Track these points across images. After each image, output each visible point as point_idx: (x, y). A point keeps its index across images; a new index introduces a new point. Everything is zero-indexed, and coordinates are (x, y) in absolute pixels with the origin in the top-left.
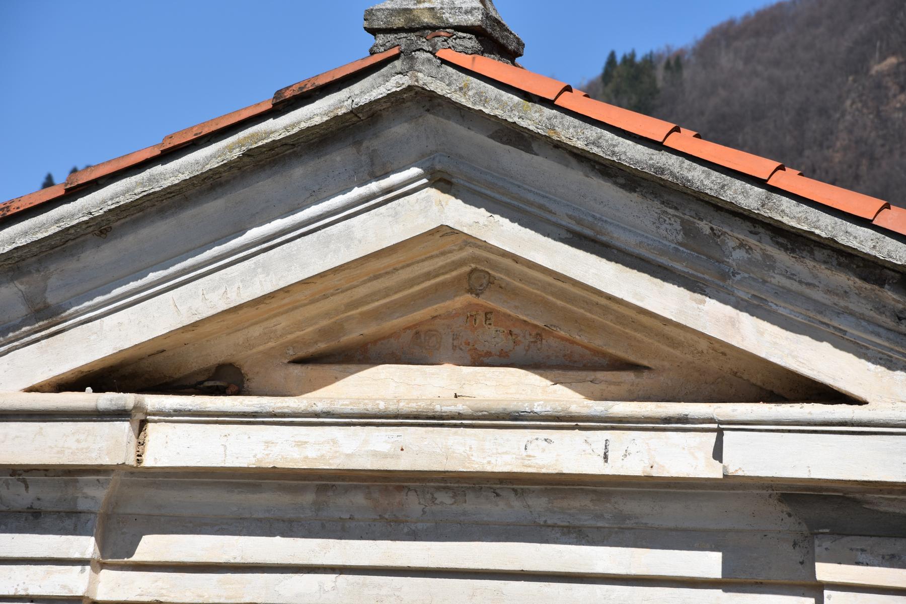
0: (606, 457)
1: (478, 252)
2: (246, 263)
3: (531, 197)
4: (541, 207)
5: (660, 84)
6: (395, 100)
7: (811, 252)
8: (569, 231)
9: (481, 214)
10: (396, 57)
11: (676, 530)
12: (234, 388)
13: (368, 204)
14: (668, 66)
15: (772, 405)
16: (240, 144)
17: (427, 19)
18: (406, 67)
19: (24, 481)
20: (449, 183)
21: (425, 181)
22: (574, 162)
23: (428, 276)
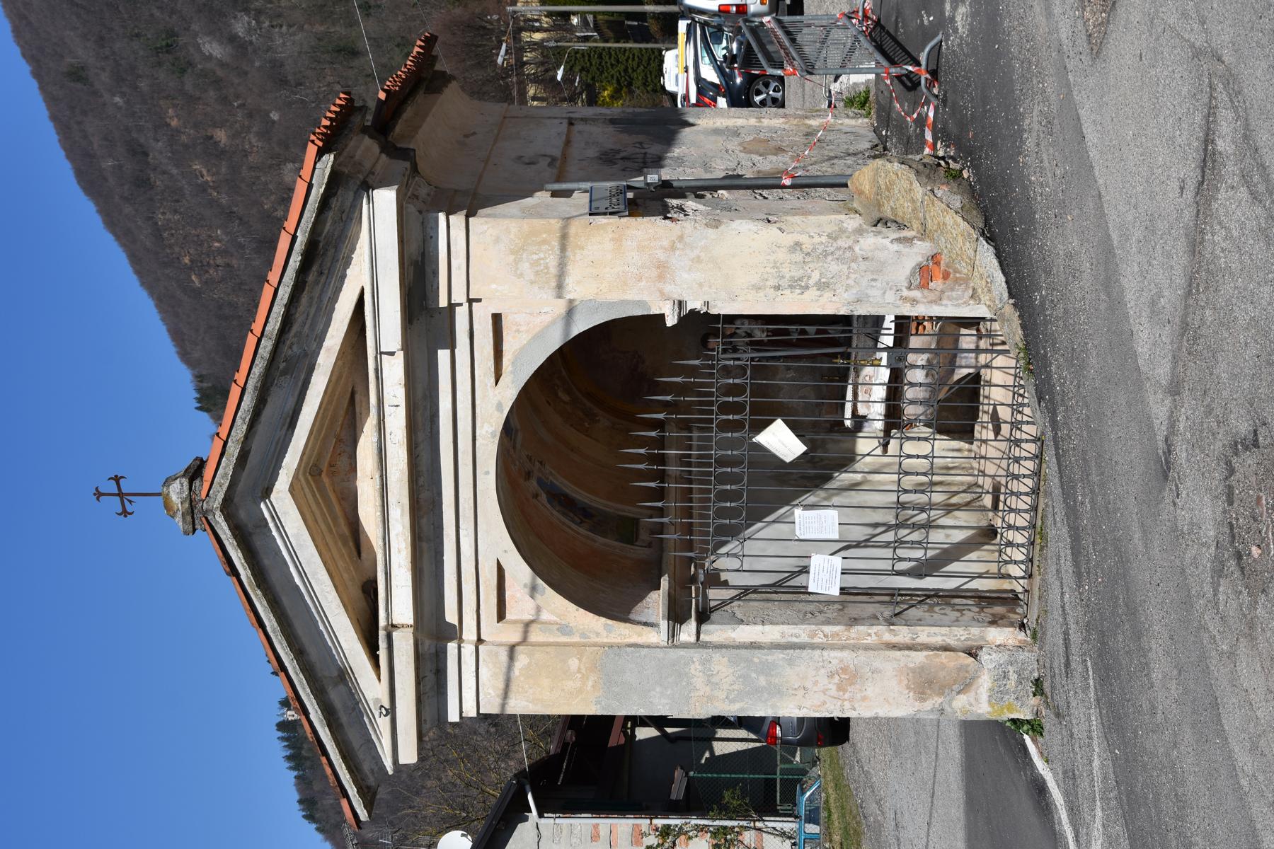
0: (397, 406)
1: (301, 472)
2: (313, 584)
3: (272, 450)
4: (277, 443)
5: (210, 385)
6: (228, 518)
7: (292, 315)
8: (288, 430)
9: (283, 473)
10: (206, 518)
11: (429, 371)
12: (374, 585)
13: (280, 527)
14: (201, 381)
15: (367, 329)
16: (254, 591)
17: (187, 505)
18: (212, 514)
19: (423, 678)
20: (267, 489)
21: (267, 501)
22: (254, 429)
23: (314, 496)
